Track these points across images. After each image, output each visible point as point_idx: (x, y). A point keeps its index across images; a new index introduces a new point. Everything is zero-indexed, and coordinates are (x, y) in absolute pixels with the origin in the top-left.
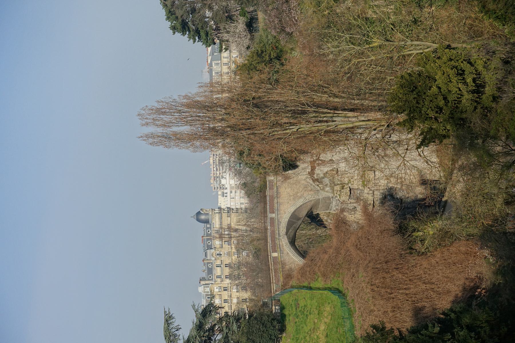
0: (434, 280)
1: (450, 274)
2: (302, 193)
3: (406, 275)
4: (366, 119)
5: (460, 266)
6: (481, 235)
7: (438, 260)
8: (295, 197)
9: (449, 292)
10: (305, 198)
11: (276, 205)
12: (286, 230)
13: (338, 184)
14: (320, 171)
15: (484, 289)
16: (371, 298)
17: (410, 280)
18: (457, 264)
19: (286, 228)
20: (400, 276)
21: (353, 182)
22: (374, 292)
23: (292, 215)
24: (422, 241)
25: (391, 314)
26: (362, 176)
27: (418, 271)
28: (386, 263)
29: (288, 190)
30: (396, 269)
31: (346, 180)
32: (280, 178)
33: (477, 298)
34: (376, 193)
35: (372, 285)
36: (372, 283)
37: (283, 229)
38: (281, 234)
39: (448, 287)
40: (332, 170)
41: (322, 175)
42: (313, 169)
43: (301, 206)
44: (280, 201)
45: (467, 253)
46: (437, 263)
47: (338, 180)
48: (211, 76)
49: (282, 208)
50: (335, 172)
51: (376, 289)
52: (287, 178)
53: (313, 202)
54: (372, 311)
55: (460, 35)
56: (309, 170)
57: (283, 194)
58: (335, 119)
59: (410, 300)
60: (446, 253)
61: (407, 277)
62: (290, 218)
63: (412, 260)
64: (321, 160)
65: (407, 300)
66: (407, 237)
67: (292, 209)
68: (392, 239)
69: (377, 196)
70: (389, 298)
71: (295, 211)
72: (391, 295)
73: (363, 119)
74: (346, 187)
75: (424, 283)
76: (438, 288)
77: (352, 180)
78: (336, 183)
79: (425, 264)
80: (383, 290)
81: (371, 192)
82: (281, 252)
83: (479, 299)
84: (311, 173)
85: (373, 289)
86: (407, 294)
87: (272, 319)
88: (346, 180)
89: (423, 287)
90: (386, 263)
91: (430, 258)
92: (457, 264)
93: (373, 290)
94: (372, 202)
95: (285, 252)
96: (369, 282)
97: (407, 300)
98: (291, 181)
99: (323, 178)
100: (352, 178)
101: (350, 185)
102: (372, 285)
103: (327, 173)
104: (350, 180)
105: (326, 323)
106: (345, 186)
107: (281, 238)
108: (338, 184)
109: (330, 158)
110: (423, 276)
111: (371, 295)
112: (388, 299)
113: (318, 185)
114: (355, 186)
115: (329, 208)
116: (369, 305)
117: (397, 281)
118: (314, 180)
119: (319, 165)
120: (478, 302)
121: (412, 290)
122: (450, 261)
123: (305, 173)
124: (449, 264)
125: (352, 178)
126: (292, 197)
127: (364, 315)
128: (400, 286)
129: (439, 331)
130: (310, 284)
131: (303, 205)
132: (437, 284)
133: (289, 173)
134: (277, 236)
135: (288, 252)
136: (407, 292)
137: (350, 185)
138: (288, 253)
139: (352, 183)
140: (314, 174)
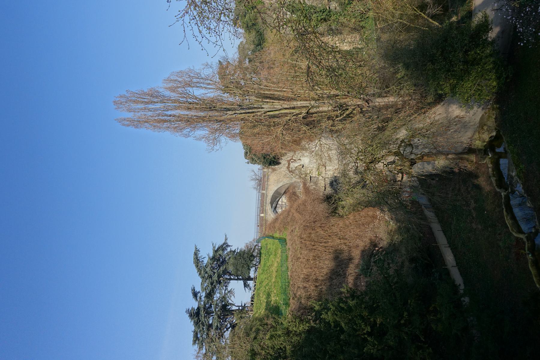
0: (347, 237)
1: (359, 233)
3: (327, 232)
4: (288, 107)
5: (368, 226)
6: (210, 132)
7: (351, 221)
8: (278, 181)
9: (357, 246)
11: (266, 186)
13: (303, 174)
14: (293, 165)
15: (381, 248)
16: (299, 248)
17: (329, 236)
18: (365, 225)
20: (322, 232)
22: (302, 244)
24: (343, 207)
25: (312, 262)
26: (318, 169)
27: (335, 229)
28: (314, 222)
29: (274, 177)
30: (320, 227)
31: (308, 172)
32: (270, 170)
33: (375, 256)
34: (326, 179)
35: (301, 238)
36: (302, 237)
39: (357, 243)
40: (300, 165)
41: (294, 169)
42: (289, 164)
43: (281, 187)
44: (269, 183)
45: (373, 217)
46: (350, 223)
49: (270, 187)
50: (301, 167)
51: (303, 242)
52: (274, 170)
53: (288, 185)
54: (300, 258)
56: (287, 165)
58: (263, 106)
59: (327, 251)
60: (357, 217)
61: (327, 234)
62: (274, 193)
63: (333, 220)
64: (293, 160)
65: (325, 251)
66: (332, 204)
67: (276, 189)
68: (321, 205)
70: (312, 249)
71: (277, 189)
72: (314, 247)
73: (286, 106)
74: (308, 175)
75: (340, 239)
76: (350, 242)
77: (312, 171)
78: (302, 173)
79: (341, 224)
80: (308, 243)
81: (323, 179)
82: (266, 213)
83: (377, 257)
84: (288, 167)
85: (301, 242)
86: (325, 247)
87: (250, 256)
88: (308, 172)
89: (338, 241)
90: (314, 222)
91: (345, 220)
92: (365, 225)
93: (301, 242)
94: (324, 185)
95: (268, 214)
96: (299, 236)
97: (325, 251)
98: (277, 172)
99: (295, 170)
101: (310, 174)
102: (301, 238)
103: (297, 167)
105: (277, 262)
108: (303, 174)
110: (339, 233)
111: (300, 246)
112: (311, 250)
113: (292, 175)
114: (314, 175)
115: (299, 188)
116: (297, 254)
117: (320, 236)
118: (290, 172)
119: (292, 162)
120: (376, 259)
121: (330, 243)
122: (360, 223)
123: (285, 167)
124: (360, 225)
126: (276, 181)
127: (293, 261)
128: (321, 240)
130: (273, 235)
131: (283, 186)
132: (349, 240)
133: (276, 168)
134: (265, 204)
136: (326, 245)
137: (310, 174)
138: (270, 214)
140: (289, 168)
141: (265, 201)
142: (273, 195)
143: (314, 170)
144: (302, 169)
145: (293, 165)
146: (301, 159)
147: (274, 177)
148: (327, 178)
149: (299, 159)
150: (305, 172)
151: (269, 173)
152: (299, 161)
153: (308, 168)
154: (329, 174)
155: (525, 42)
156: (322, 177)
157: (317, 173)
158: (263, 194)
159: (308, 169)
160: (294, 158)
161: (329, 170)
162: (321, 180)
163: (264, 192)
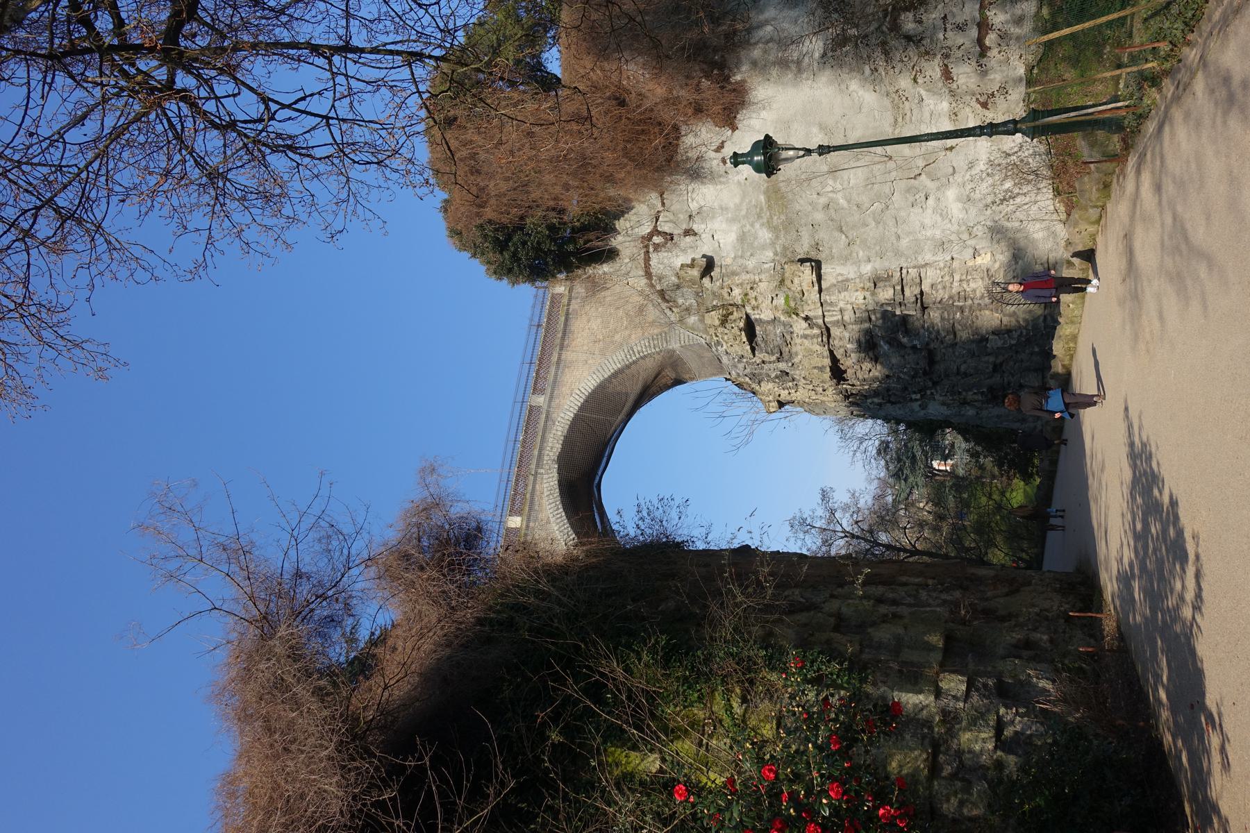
2: (627, 332)
10: (632, 348)
12: (560, 446)
19: (561, 442)
21: (756, 299)
23: (586, 401)
32: (580, 289)
34: (835, 332)
37: (554, 445)
38: (546, 458)
44: (568, 355)
47: (714, 293)
48: (813, 337)
50: (695, 273)
52: (596, 287)
55: (552, 643)
57: (580, 335)
62: (582, 408)
69: (841, 343)
77: (752, 294)
81: (816, 331)
95: (541, 516)
100: (752, 288)
104: (746, 295)
106: (732, 313)
107: (542, 471)
109: (684, 226)
119: (657, 247)
125: (752, 288)
129: (1013, 754)
131: (628, 367)
135: (551, 516)
137: (749, 310)
139: (753, 302)
141: (536, 452)
142: (576, 416)
143: (763, 286)
144: (706, 281)
145: (670, 262)
146: (695, 227)
147: (595, 324)
148: (836, 323)
149: (689, 232)
150: (720, 297)
151: (575, 305)
152: (688, 239)
153: (734, 273)
154: (841, 304)
155: (866, 808)
156: (804, 325)
157: (781, 301)
158: (533, 411)
159: (737, 280)
160: (665, 228)
161: (843, 285)
162: (805, 337)
163: (540, 400)
